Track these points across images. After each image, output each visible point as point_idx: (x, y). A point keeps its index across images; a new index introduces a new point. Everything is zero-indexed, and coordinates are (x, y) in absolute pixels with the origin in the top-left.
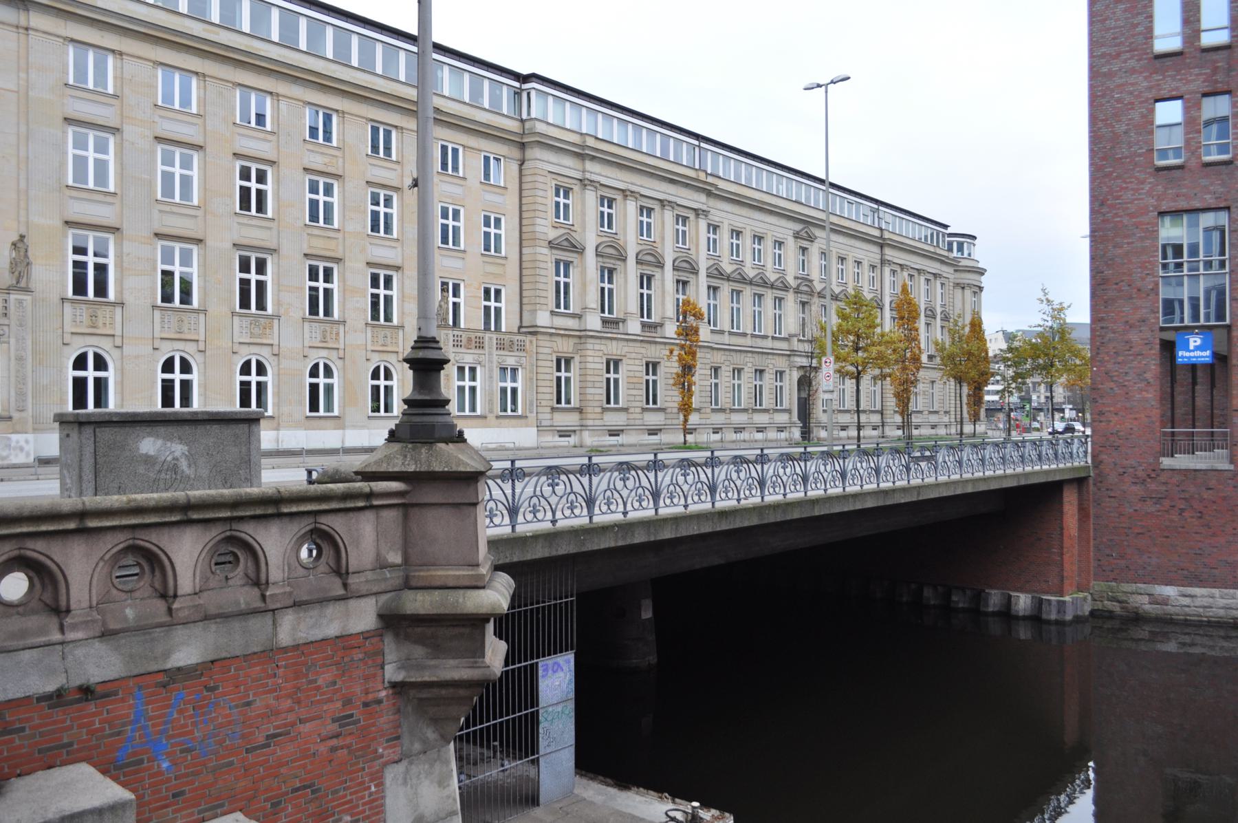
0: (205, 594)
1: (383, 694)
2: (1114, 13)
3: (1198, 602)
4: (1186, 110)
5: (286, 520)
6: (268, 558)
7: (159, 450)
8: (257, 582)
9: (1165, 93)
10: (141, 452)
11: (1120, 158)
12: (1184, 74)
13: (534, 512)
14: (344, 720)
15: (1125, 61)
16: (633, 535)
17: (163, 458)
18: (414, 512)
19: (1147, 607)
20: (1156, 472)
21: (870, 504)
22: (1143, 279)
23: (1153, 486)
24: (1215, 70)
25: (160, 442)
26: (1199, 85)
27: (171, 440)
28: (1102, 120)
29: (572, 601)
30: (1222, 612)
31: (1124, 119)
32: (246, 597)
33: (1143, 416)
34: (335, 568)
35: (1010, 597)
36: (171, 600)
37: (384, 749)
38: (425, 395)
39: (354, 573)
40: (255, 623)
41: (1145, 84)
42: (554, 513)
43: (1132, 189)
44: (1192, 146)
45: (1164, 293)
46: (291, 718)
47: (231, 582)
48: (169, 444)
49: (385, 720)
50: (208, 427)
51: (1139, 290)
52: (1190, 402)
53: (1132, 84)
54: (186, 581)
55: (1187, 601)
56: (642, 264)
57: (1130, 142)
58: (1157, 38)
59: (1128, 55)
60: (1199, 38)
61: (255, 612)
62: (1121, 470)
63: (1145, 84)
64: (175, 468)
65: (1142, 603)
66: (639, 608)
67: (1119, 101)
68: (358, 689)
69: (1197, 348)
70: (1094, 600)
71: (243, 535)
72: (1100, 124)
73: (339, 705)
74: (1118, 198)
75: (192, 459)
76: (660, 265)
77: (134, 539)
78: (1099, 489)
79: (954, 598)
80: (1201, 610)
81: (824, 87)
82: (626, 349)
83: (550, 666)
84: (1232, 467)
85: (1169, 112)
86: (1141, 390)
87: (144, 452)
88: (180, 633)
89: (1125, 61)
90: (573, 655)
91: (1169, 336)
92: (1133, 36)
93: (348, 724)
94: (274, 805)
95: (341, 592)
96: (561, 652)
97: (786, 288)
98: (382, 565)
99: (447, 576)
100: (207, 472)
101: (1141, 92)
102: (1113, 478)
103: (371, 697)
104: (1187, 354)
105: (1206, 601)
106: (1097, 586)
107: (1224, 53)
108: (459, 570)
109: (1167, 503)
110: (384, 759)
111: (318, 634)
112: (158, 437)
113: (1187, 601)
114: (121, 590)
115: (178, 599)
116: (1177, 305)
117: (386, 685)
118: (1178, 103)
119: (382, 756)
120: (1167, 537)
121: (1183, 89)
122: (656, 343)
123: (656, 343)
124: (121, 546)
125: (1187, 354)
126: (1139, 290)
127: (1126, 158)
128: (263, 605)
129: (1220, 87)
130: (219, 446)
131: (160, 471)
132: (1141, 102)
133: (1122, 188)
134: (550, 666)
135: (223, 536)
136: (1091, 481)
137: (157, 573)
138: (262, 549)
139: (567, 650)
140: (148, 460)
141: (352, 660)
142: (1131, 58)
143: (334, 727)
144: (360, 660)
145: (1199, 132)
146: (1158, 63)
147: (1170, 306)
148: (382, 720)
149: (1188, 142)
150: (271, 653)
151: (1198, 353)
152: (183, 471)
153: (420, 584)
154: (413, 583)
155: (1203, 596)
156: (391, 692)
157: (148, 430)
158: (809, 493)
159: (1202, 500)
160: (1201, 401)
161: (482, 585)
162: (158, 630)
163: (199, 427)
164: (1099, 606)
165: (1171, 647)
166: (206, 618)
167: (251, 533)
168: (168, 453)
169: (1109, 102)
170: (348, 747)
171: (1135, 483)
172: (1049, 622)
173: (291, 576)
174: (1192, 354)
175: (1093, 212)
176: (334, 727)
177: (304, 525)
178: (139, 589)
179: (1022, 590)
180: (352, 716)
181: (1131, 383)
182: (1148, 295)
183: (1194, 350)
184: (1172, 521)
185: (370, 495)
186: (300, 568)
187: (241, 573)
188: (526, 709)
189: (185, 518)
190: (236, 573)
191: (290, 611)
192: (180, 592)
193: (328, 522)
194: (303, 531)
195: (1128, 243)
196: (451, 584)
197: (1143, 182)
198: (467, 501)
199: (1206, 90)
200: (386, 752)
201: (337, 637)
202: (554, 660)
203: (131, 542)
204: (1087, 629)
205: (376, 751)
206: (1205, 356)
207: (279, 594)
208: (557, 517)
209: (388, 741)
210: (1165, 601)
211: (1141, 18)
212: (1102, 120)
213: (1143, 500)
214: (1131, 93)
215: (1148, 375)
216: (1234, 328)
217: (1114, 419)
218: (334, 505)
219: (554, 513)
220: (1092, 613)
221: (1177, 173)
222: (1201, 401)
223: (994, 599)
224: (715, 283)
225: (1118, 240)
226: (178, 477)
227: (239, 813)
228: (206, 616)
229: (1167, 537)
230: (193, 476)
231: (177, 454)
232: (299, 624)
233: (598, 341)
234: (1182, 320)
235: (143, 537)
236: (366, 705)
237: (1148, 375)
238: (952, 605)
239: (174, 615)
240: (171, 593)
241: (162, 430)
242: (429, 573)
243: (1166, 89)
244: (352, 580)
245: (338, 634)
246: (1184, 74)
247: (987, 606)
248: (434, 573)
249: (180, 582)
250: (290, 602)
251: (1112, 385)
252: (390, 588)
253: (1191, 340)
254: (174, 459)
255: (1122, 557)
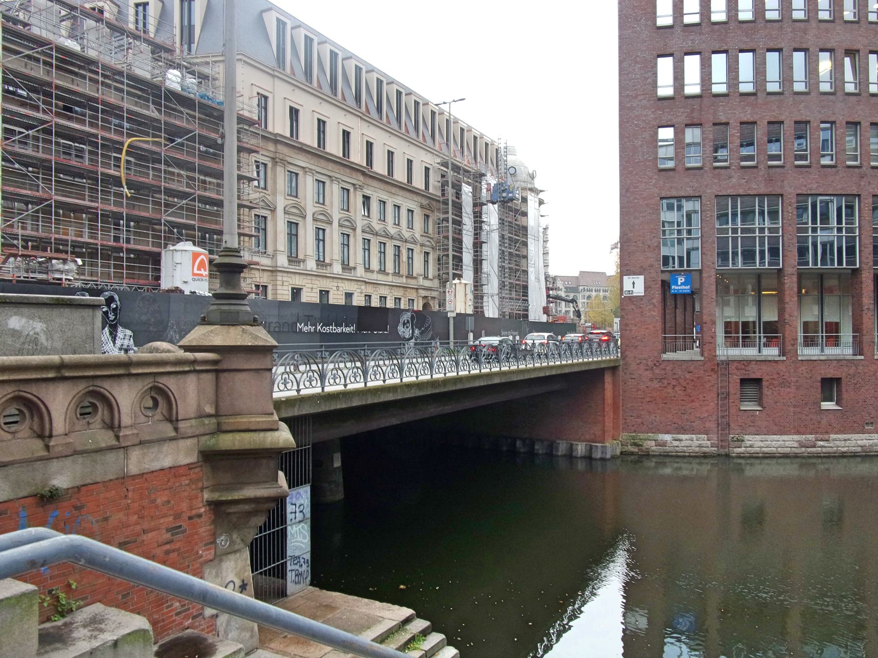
0: (73, 435)
1: (203, 510)
2: (634, 70)
3: (683, 443)
4: (676, 133)
5: (133, 379)
6: (121, 408)
7: (23, 326)
8: (112, 425)
9: (664, 123)
10: (9, 327)
11: (638, 162)
12: (676, 111)
13: (285, 384)
14: (174, 530)
15: (640, 101)
16: (351, 400)
17: (27, 333)
18: (224, 376)
19: (654, 448)
20: (658, 363)
21: (497, 381)
22: (651, 240)
23: (657, 371)
24: (693, 110)
25: (24, 320)
26: (682, 119)
27: (33, 318)
28: (627, 137)
29: (309, 448)
30: (697, 449)
31: (640, 137)
32: (105, 438)
33: (651, 326)
34: (167, 416)
35: (572, 445)
36: (47, 439)
37: (203, 551)
38: (230, 289)
39: (181, 420)
40: (111, 457)
41: (652, 116)
42: (298, 385)
43: (645, 182)
44: (679, 156)
45: (664, 251)
46: (138, 528)
47: (91, 426)
48: (31, 322)
49: (204, 528)
50: (62, 310)
51: (649, 247)
52: (673, 320)
53: (645, 116)
54: (59, 425)
55: (676, 443)
56: (316, 221)
57: (643, 152)
58: (660, 87)
59: (642, 97)
60: (683, 90)
61: (111, 448)
62: (639, 361)
63: (652, 116)
64: (35, 341)
65: (650, 445)
66: (332, 462)
67: (637, 125)
68: (184, 506)
69: (682, 284)
70: (622, 445)
71: (102, 390)
72: (626, 140)
73: (171, 519)
74: (636, 187)
75: (49, 334)
76: (330, 223)
77: (20, 391)
78: (625, 374)
79: (537, 447)
80: (685, 448)
81: (448, 104)
82: (305, 281)
83: (294, 495)
84: (703, 358)
85: (667, 134)
86: (650, 310)
87: (12, 327)
88: (55, 465)
89: (640, 101)
90: (309, 487)
91: (666, 277)
92: (645, 85)
93: (177, 533)
94: (124, 596)
95: (173, 434)
96: (301, 485)
97: (415, 242)
98: (201, 416)
99: (250, 422)
100: (61, 344)
101: (650, 121)
102: (633, 366)
103: (194, 512)
104: (677, 288)
105: (688, 443)
106: (624, 436)
107: (698, 100)
108: (259, 417)
109: (665, 382)
110: (203, 559)
111: (157, 465)
112: (22, 315)
113: (676, 443)
114: (8, 432)
115: (53, 439)
116: (671, 259)
117: (205, 503)
118: (672, 129)
119: (201, 556)
120: (666, 403)
121: (675, 121)
122: (327, 277)
123: (327, 277)
124: (9, 396)
125: (677, 288)
126: (649, 247)
127: (641, 162)
128: (117, 443)
129: (696, 121)
130: (70, 325)
131: (24, 343)
132: (651, 128)
133: (639, 181)
134: (294, 495)
135: (87, 390)
136: (621, 368)
137: (36, 419)
138: (116, 401)
139: (305, 483)
140: (15, 333)
141: (181, 485)
142: (644, 99)
143: (168, 536)
144: (187, 485)
145: (684, 148)
146: (660, 103)
147: (666, 260)
148: (202, 530)
149: (676, 154)
150: (124, 479)
151: (683, 287)
152: (42, 344)
153: (229, 428)
154: (225, 427)
155: (686, 440)
156: (208, 508)
157: (15, 310)
158: (460, 373)
159: (686, 379)
160: (680, 319)
161: (276, 428)
162: (39, 463)
163: (55, 310)
164: (626, 449)
165: (668, 471)
166: (76, 453)
167: (108, 388)
168: (30, 329)
169: (631, 126)
170: (178, 550)
171: (646, 370)
172: (596, 459)
173: (136, 422)
174: (680, 288)
175: (622, 196)
176: (168, 536)
177: (148, 383)
178: (21, 431)
179: (580, 440)
180: (180, 527)
181: (644, 306)
182: (654, 250)
183: (680, 286)
184: (668, 393)
185: (194, 362)
186: (143, 416)
187: (99, 420)
188: (278, 526)
189: (59, 375)
190: (95, 419)
191: (137, 448)
192: (54, 433)
193: (164, 381)
194: (146, 388)
195: (642, 216)
196: (253, 428)
197: (651, 178)
198: (263, 367)
199: (689, 122)
200: (204, 553)
201: (170, 468)
202: (296, 491)
203: (16, 393)
204: (618, 462)
205: (197, 553)
206: (687, 289)
207: (129, 435)
208: (300, 388)
209: (205, 545)
210: (664, 444)
211: (650, 74)
212: (627, 137)
213: (651, 380)
214: (644, 121)
215: (654, 301)
216: (704, 272)
217: (634, 328)
218: (169, 369)
219: (298, 385)
220: (622, 453)
221: (671, 173)
222: (680, 319)
223: (562, 448)
224: (368, 236)
225: (637, 214)
226: (39, 348)
227: (98, 604)
228: (75, 451)
229: (666, 403)
230: (50, 347)
231: (38, 330)
232: (143, 458)
233: (285, 275)
234: (674, 267)
235: (26, 390)
236: (190, 518)
237: (654, 301)
238: (536, 451)
239: (51, 450)
240: (47, 433)
241: (26, 310)
242: (236, 420)
243: (665, 120)
244: (182, 425)
245: (170, 465)
246: (676, 111)
247: (557, 451)
248: (241, 420)
249: (54, 425)
250: (137, 441)
251: (633, 307)
252: (208, 432)
253: (679, 279)
254: (35, 333)
255: (638, 417)
